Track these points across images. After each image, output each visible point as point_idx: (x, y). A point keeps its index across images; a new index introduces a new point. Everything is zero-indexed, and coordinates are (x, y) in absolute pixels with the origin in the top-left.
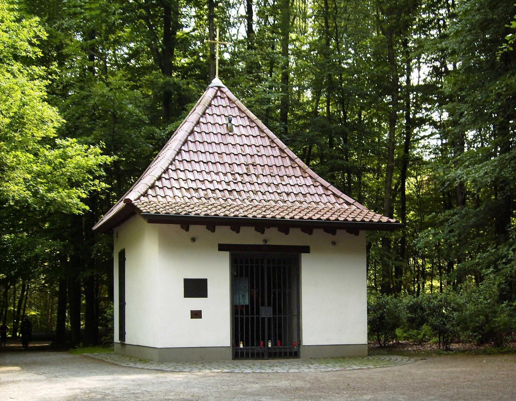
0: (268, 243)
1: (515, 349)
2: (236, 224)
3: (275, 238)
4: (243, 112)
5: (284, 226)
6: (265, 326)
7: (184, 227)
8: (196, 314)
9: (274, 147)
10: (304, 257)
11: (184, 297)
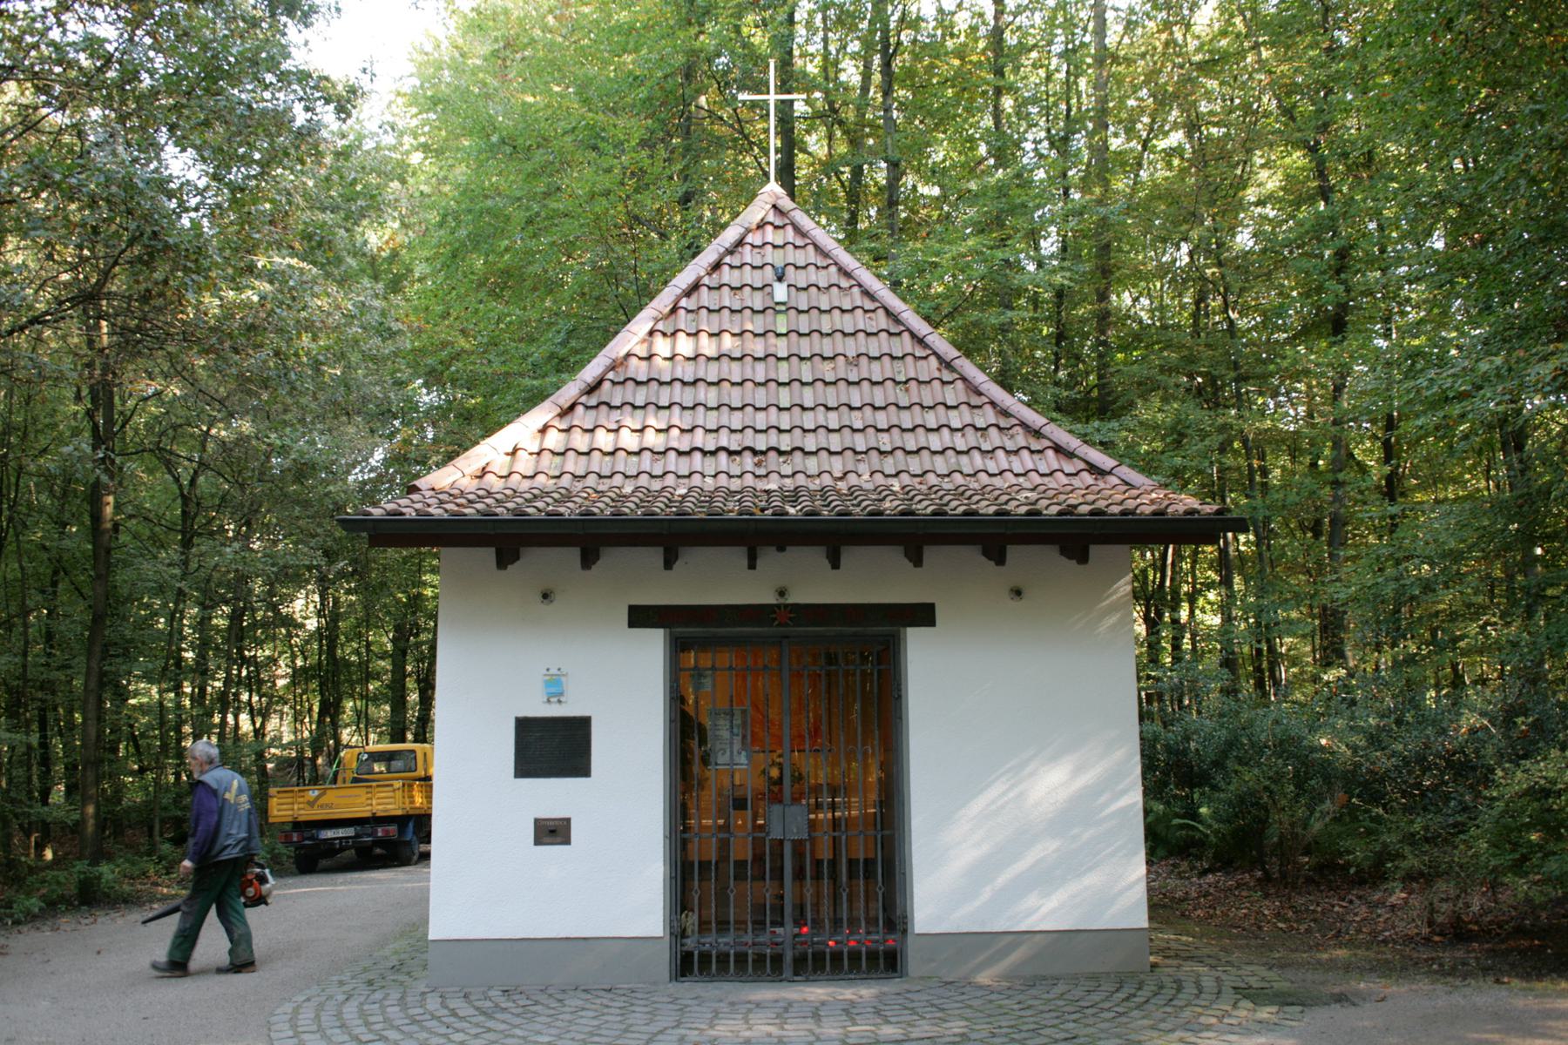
0: (792, 599)
1: (442, 4)
2: (673, 534)
3: (815, 584)
4: (1070, 455)
5: (836, 534)
6: (793, 860)
8: (552, 832)
9: (899, 334)
10: (918, 648)
11: (516, 776)
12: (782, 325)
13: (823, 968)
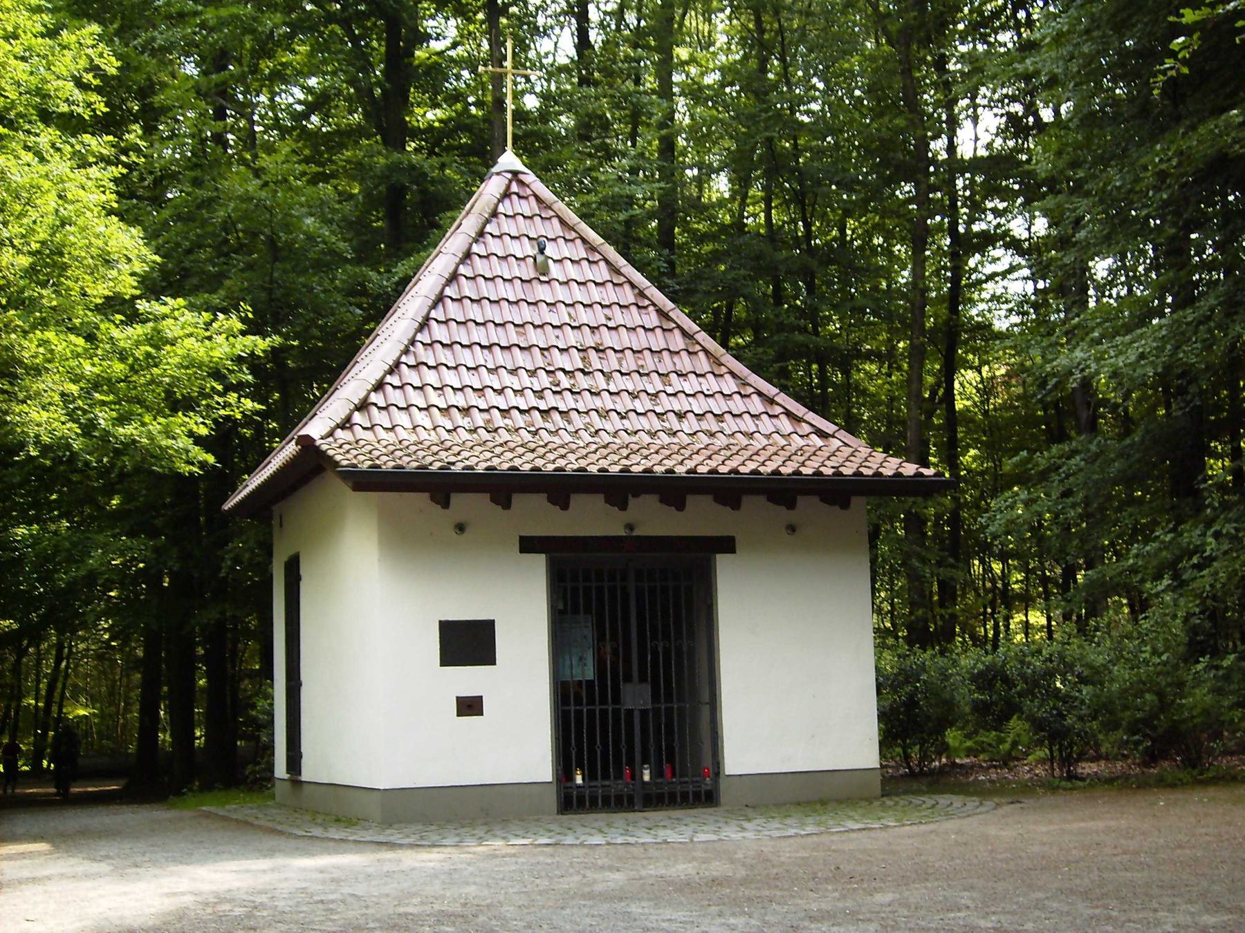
0: (636, 533)
2: (561, 488)
3: (654, 520)
4: (572, 229)
5: (673, 490)
6: (634, 730)
7: (435, 499)
8: (470, 706)
12: (612, 361)
13: (663, 803)
